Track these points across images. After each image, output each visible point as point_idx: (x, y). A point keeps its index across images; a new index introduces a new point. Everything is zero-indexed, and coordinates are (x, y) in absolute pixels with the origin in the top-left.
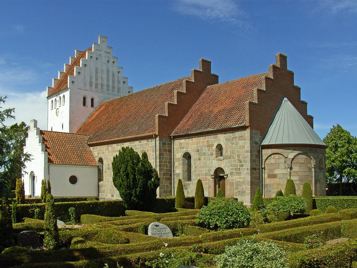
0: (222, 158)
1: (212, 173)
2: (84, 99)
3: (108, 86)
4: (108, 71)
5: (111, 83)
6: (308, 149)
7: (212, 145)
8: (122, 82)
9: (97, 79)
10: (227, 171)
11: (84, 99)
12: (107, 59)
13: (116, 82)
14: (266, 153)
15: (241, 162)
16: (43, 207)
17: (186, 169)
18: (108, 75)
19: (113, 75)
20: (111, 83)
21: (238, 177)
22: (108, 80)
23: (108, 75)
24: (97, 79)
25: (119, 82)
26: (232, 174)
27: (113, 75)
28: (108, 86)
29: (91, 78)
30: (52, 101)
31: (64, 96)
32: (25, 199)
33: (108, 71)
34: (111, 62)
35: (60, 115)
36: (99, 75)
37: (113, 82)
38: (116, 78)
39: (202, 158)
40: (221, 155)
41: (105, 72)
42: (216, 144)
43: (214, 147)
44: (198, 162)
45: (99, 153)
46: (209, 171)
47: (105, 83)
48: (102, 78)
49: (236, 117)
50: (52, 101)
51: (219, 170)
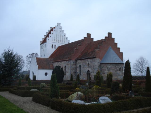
0: (89, 67)
1: (87, 72)
2: (52, 45)
3: (61, 40)
4: (61, 35)
5: (62, 39)
6: (115, 64)
7: (87, 63)
8: (66, 39)
9: (57, 38)
10: (91, 71)
11: (52, 45)
12: (60, 31)
13: (64, 39)
14: (103, 65)
15: (94, 69)
16: (97, 100)
17: (110, 64)
18: (61, 37)
19: (63, 37)
20: (62, 39)
21: (93, 73)
22: (61, 38)
23: (61, 37)
24: (57, 38)
25: (65, 39)
26: (92, 72)
27: (63, 37)
28: (61, 40)
29: (55, 38)
30: (42, 46)
31: (45, 45)
32: (81, 79)
33: (61, 35)
34: (62, 32)
35: (44, 51)
36: (58, 37)
37: (63, 39)
38: (64, 38)
39: (84, 67)
40: (89, 66)
41: (60, 36)
42: (88, 63)
43: (87, 64)
44: (83, 68)
45: (55, 65)
46: (86, 71)
47: (60, 39)
48: (59, 38)
49: (93, 54)
50: (42, 46)
51: (88, 71)
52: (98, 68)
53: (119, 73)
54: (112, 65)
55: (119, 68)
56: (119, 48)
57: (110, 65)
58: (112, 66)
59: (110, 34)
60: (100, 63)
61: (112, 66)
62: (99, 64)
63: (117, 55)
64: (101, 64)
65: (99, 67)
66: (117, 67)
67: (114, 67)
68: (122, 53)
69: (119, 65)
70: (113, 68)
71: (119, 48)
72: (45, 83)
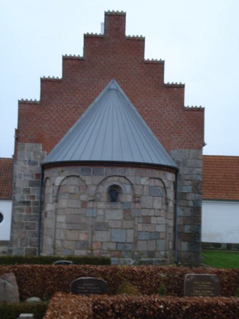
6: (80, 168)
14: (57, 178)
52: (27, 191)
53: (101, 212)
54: (68, 171)
55: (107, 186)
56: (179, 89)
57: (59, 175)
58: (68, 177)
59: (115, 20)
60: (39, 166)
61: (68, 177)
62: (37, 169)
63: (144, 116)
64: (45, 167)
65: (32, 184)
66: (89, 180)
67: (74, 181)
68: (199, 112)
69: (105, 170)
70: (72, 190)
71: (179, 89)
72: (117, 257)
